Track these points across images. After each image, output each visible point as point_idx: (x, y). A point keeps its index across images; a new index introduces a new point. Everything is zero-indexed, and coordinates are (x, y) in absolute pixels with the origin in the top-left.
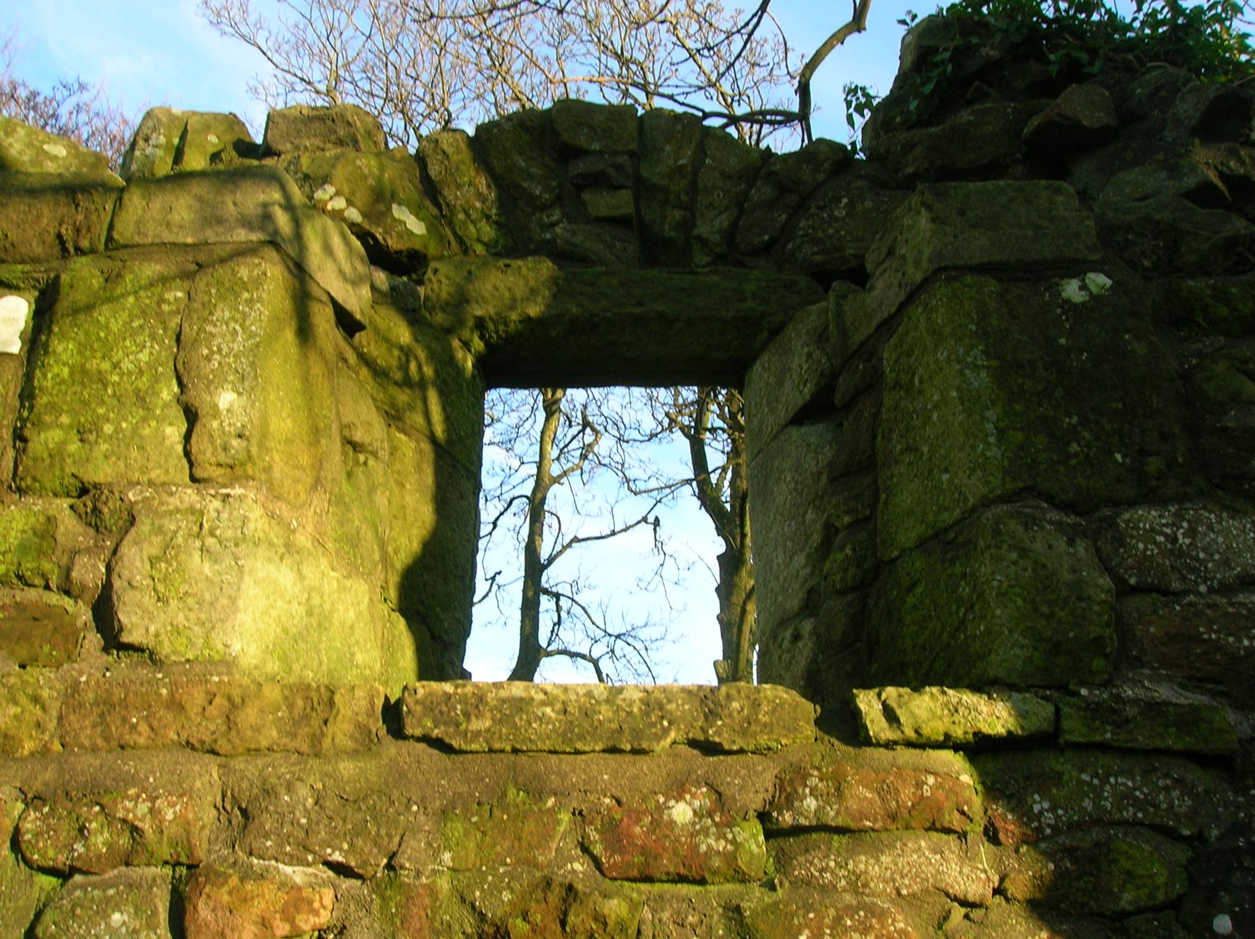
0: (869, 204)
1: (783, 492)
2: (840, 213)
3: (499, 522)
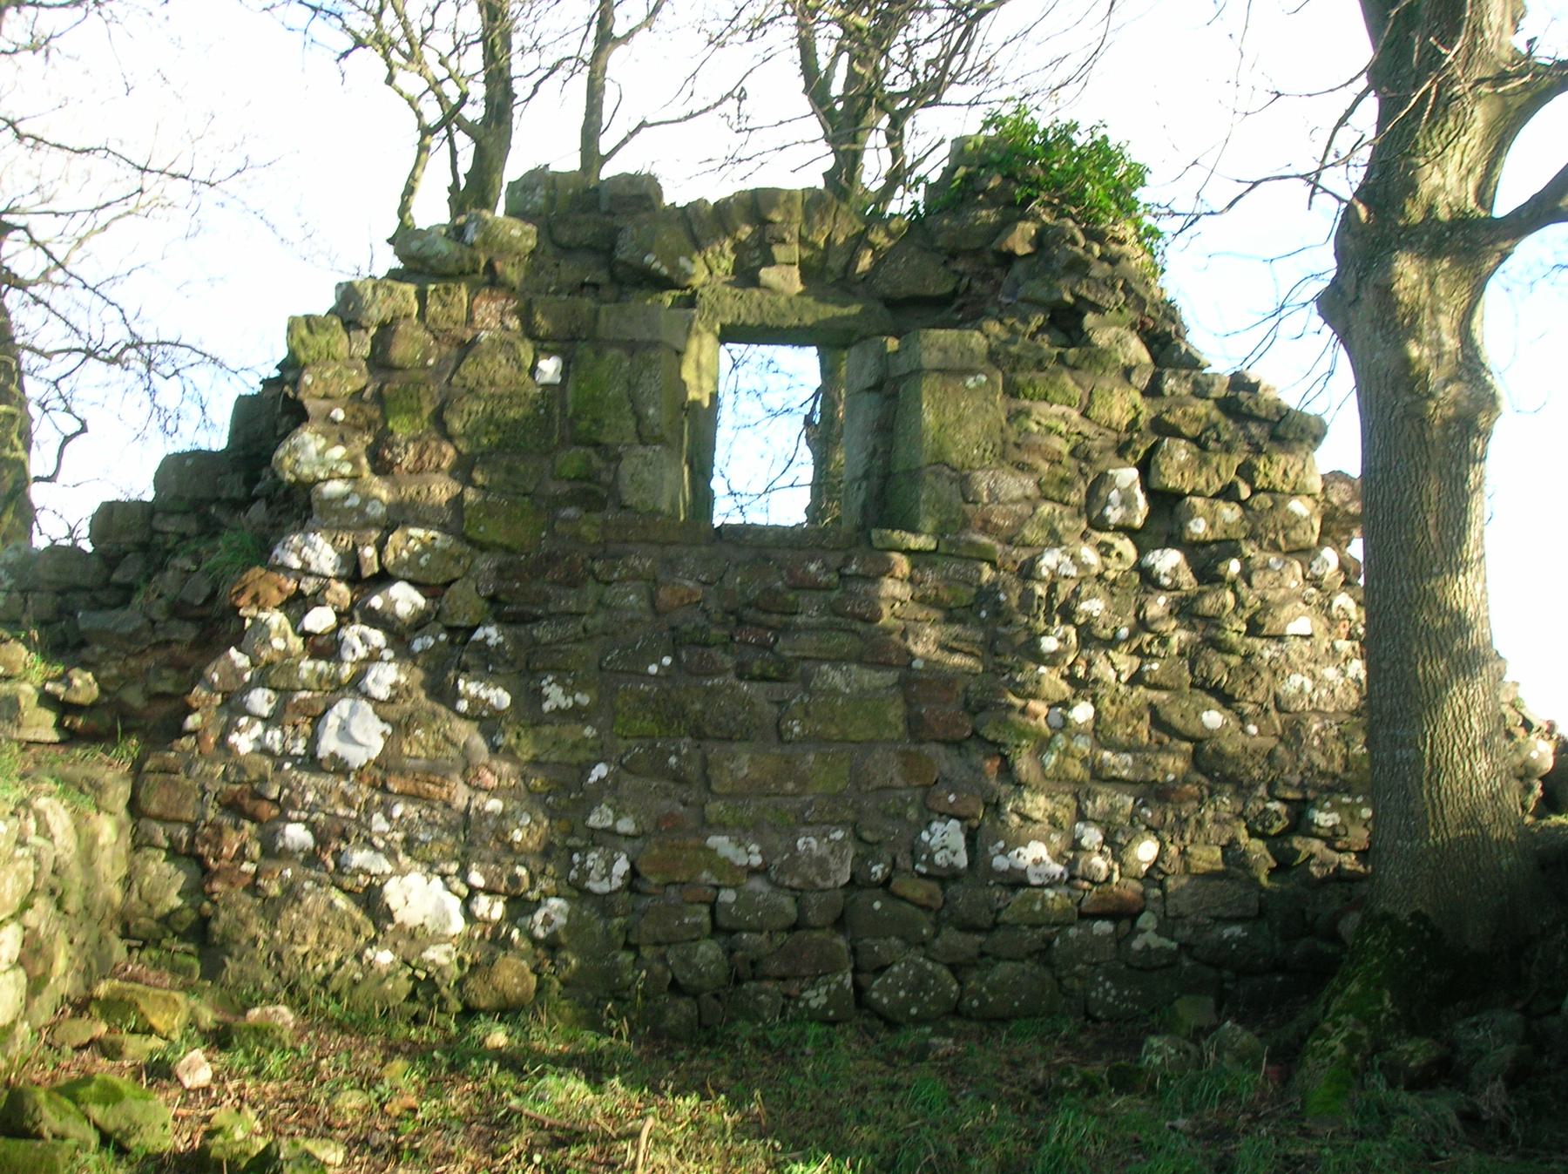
0: (916, 261)
1: (859, 421)
2: (901, 266)
3: (541, 87)
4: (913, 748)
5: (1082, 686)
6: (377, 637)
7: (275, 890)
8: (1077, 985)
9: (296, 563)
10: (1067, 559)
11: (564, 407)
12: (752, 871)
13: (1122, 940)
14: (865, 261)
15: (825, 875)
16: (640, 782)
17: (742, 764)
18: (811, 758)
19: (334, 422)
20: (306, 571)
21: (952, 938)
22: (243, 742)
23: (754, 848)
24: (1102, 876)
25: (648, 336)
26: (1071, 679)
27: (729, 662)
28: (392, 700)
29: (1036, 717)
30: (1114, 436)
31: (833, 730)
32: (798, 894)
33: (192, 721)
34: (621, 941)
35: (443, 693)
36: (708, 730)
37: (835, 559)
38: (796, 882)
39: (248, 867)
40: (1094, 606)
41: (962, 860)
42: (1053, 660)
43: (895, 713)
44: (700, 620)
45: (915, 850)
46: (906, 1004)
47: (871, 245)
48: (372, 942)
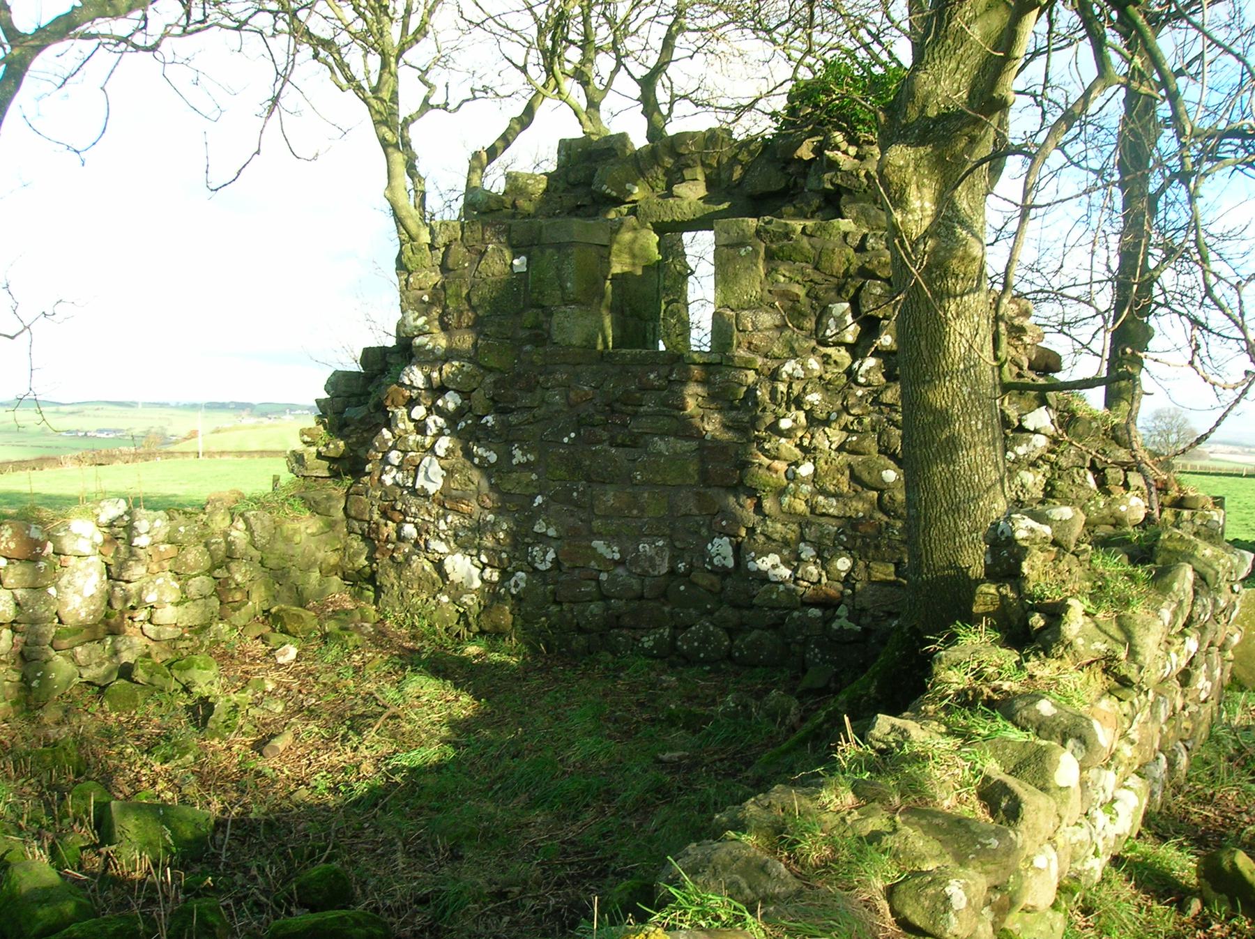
4: (702, 490)
5: (808, 451)
6: (441, 421)
7: (401, 558)
8: (798, 649)
9: (408, 382)
10: (799, 366)
11: (526, 285)
12: (617, 563)
13: (827, 621)
14: (738, 172)
15: (653, 566)
16: (558, 507)
17: (610, 498)
18: (646, 495)
19: (424, 302)
20: (412, 387)
21: (728, 613)
22: (388, 480)
23: (616, 549)
24: (815, 579)
25: (567, 239)
26: (800, 446)
27: (605, 435)
28: (446, 458)
29: (776, 472)
30: (835, 281)
31: (658, 478)
32: (643, 576)
33: (369, 467)
34: (551, 599)
35: (468, 454)
36: (594, 477)
37: (664, 371)
38: (639, 570)
39: (390, 546)
40: (814, 398)
41: (730, 563)
42: (788, 434)
43: (692, 468)
44: (591, 410)
45: (704, 554)
46: (698, 650)
47: (740, 162)
48: (440, 590)
